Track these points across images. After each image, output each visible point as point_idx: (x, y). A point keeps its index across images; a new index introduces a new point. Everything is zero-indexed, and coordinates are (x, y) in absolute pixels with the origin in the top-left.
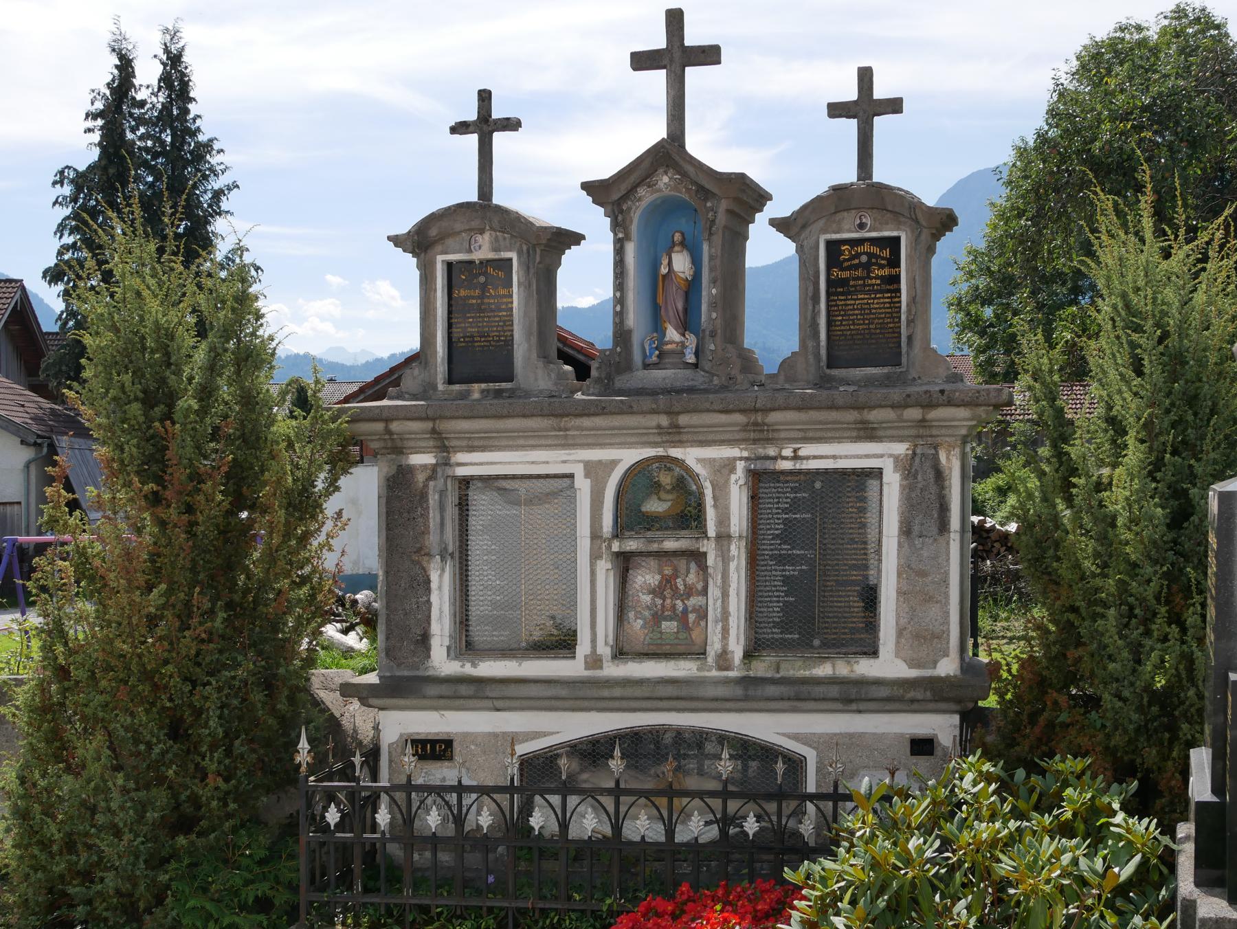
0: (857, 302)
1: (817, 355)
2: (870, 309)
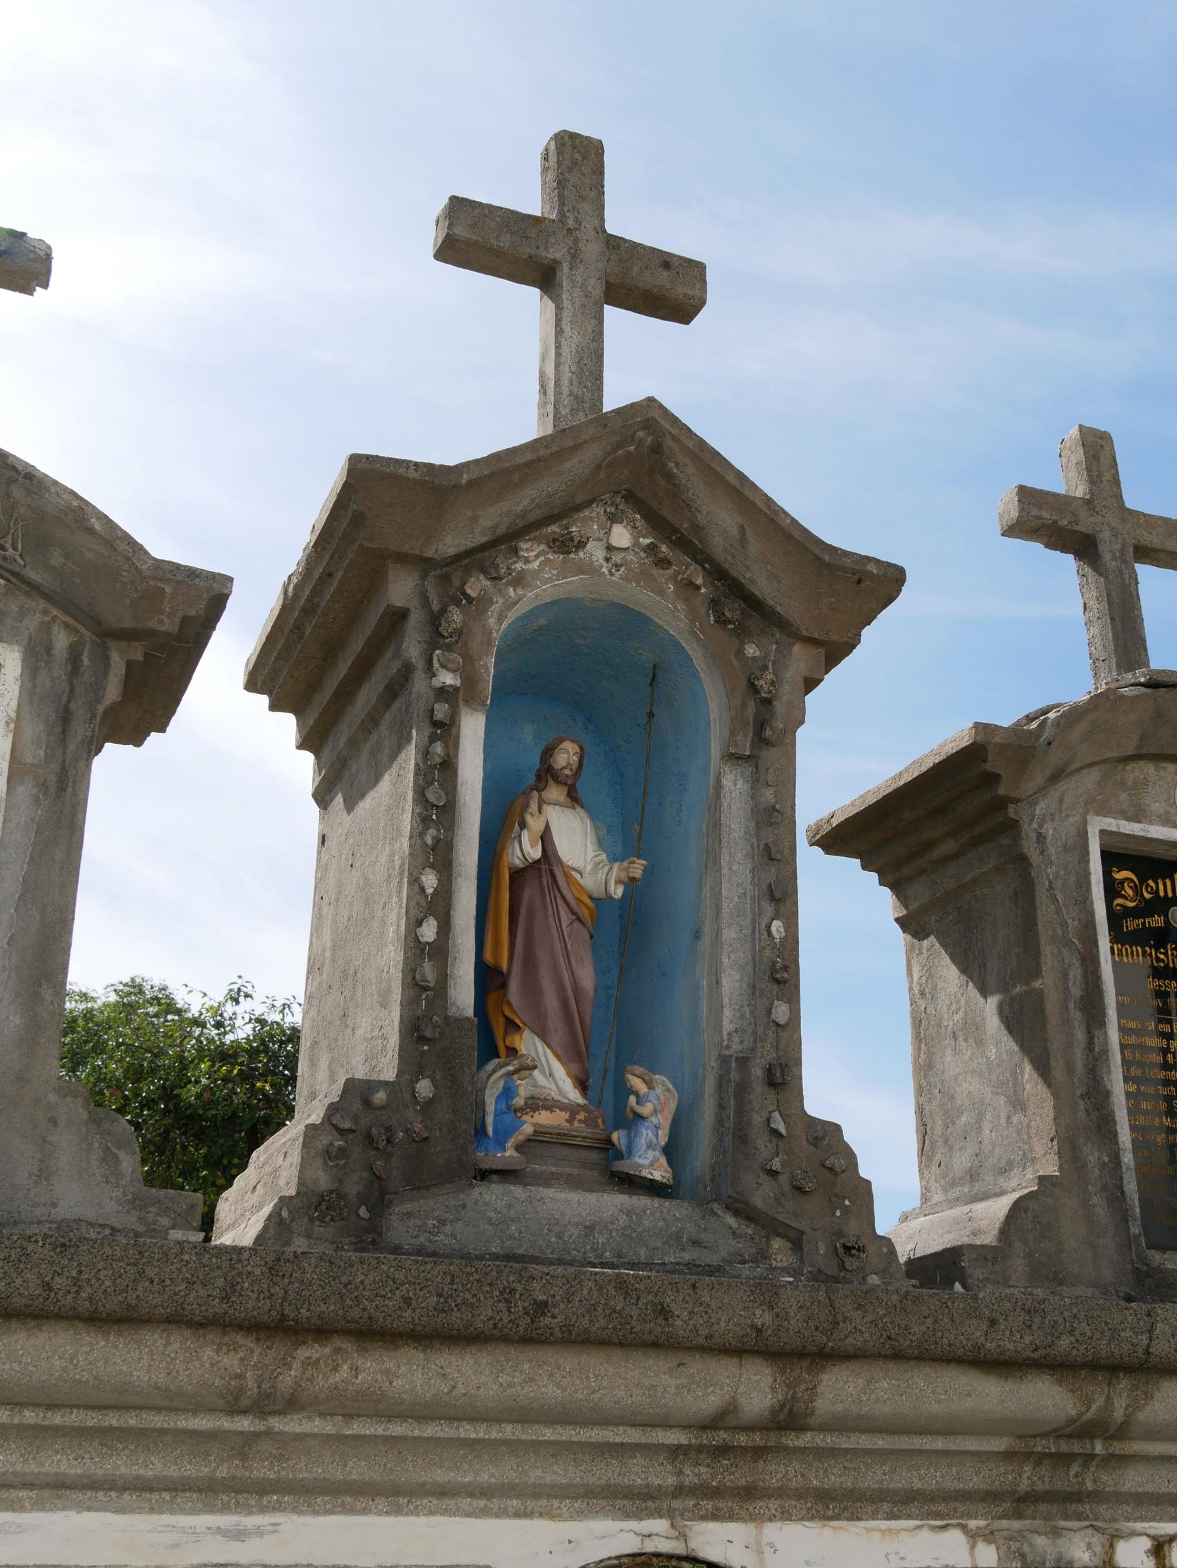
1: (1117, 1196)
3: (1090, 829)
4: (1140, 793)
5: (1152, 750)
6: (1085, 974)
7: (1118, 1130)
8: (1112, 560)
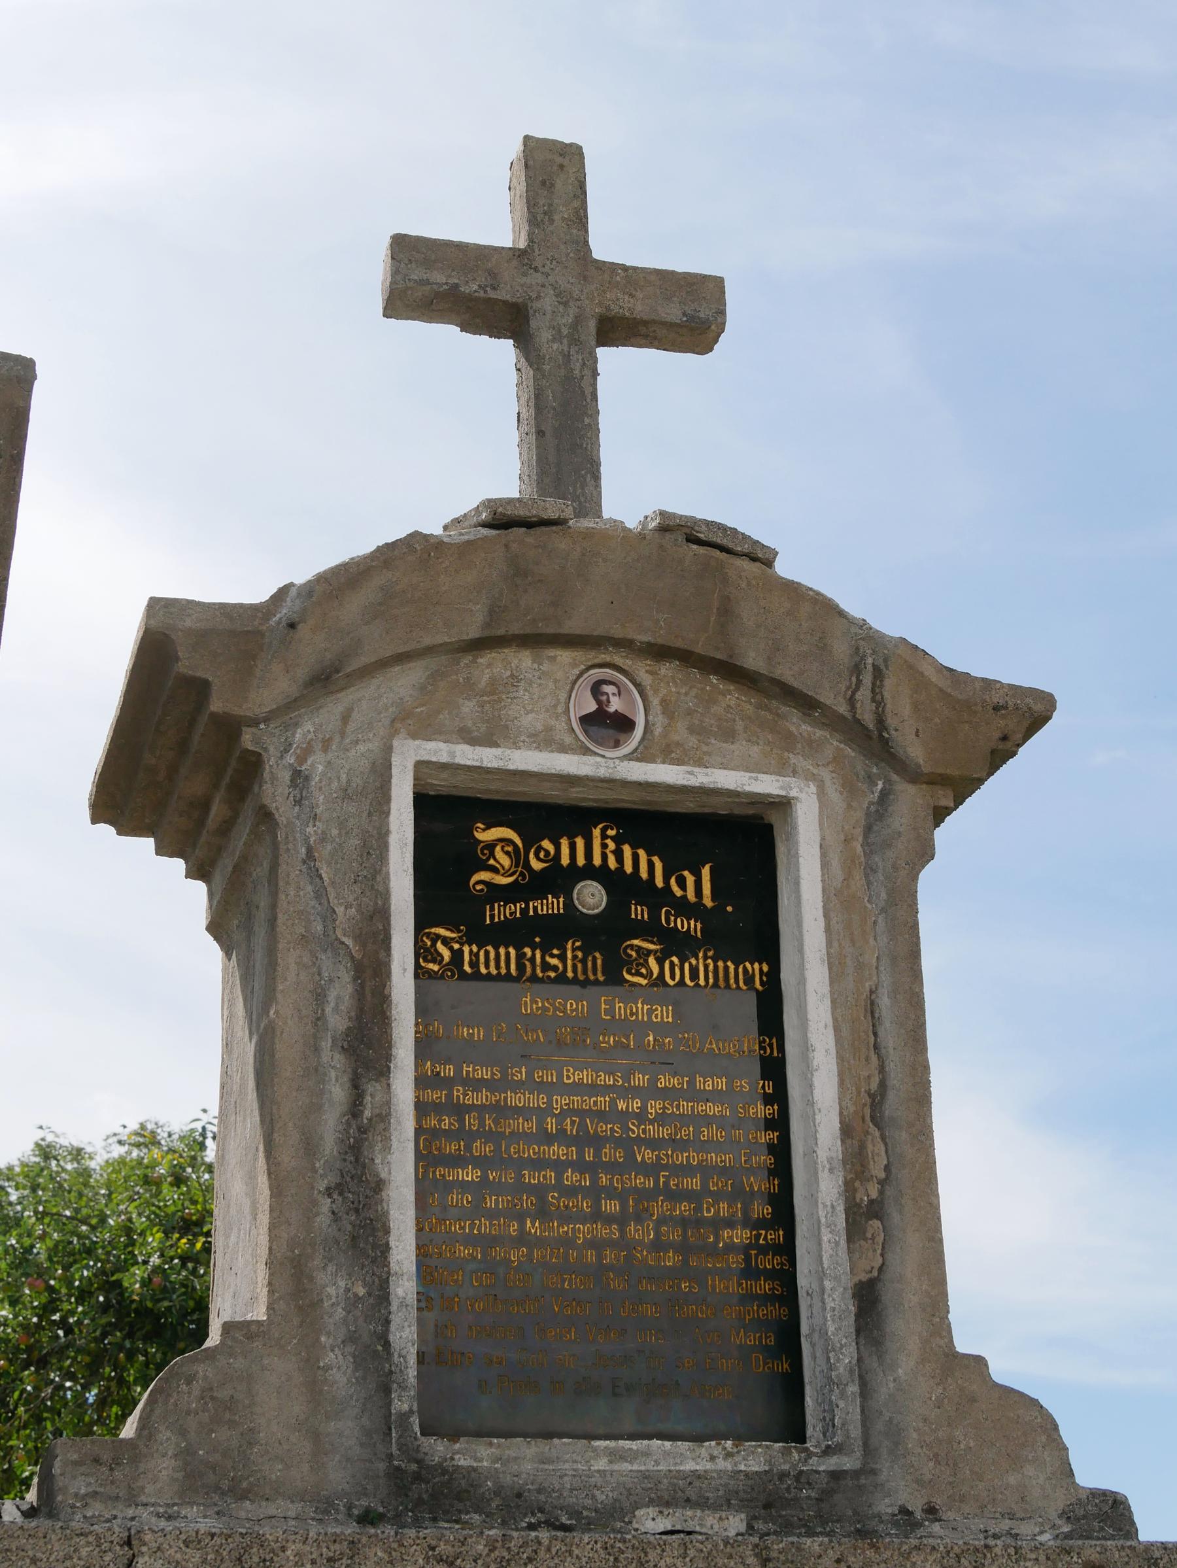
0: (561, 1102)
2: (627, 1144)
3: (396, 760)
4: (500, 700)
5: (516, 629)
6: (360, 993)
7: (392, 1244)
8: (554, 340)
